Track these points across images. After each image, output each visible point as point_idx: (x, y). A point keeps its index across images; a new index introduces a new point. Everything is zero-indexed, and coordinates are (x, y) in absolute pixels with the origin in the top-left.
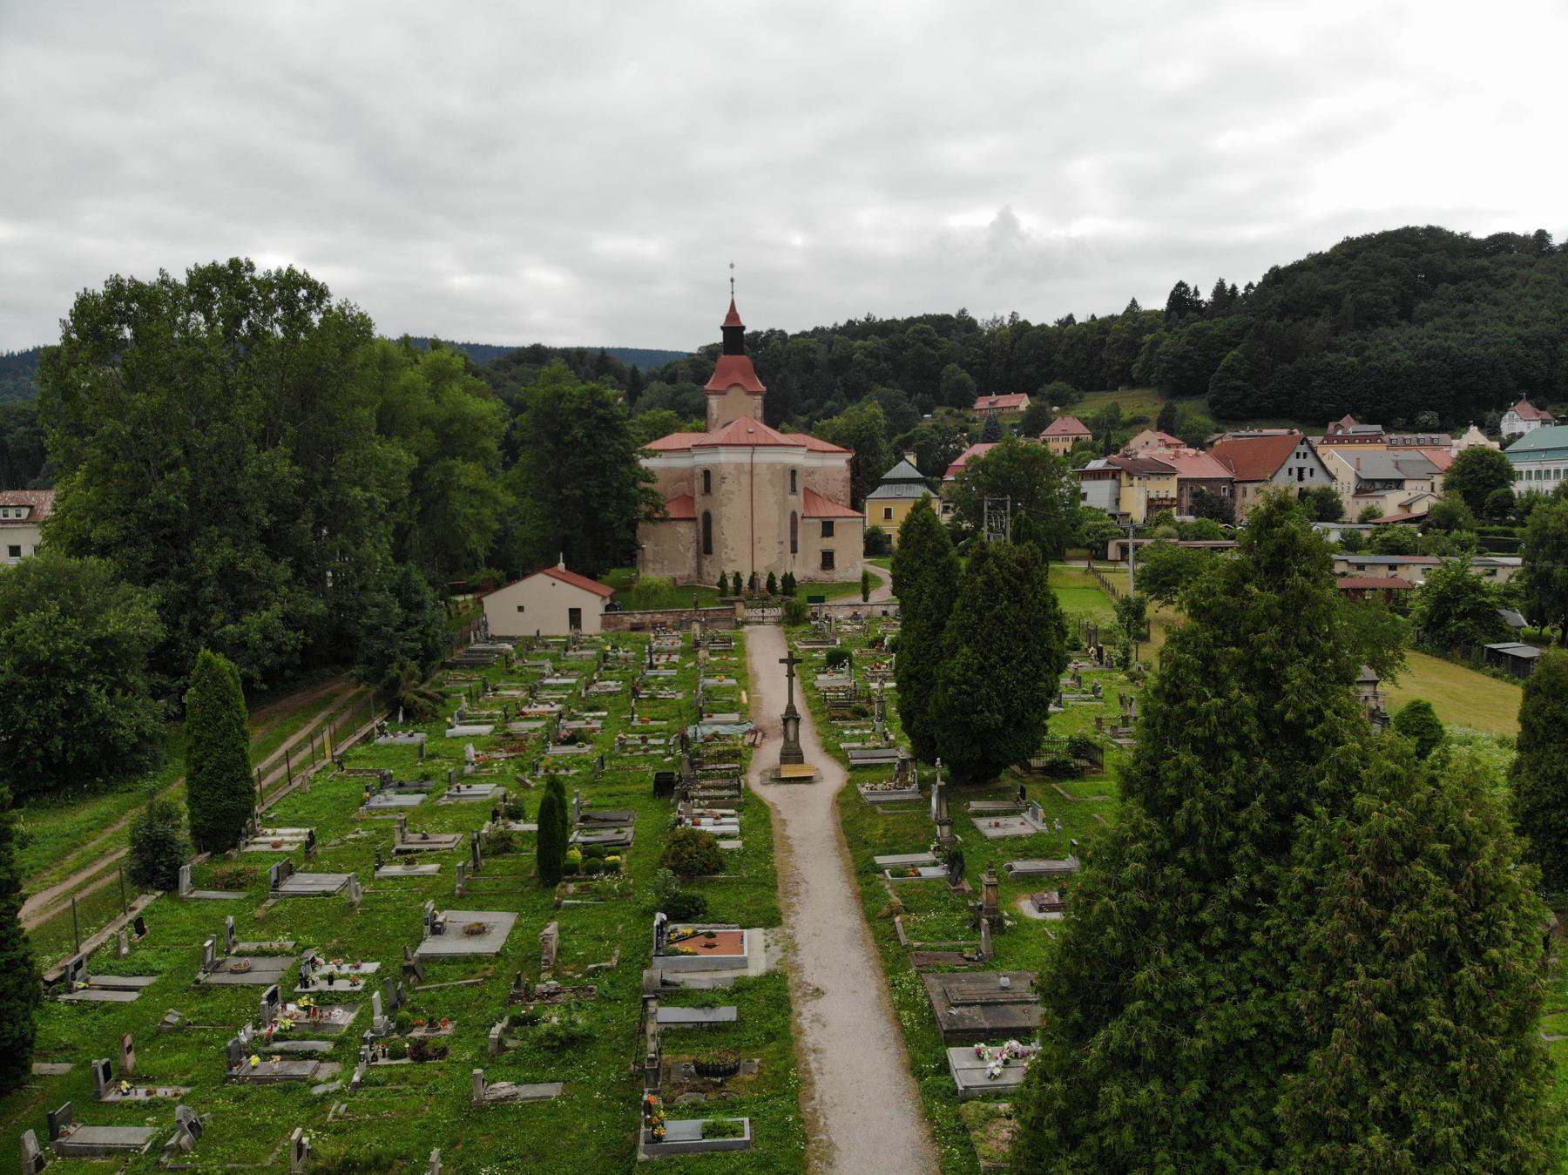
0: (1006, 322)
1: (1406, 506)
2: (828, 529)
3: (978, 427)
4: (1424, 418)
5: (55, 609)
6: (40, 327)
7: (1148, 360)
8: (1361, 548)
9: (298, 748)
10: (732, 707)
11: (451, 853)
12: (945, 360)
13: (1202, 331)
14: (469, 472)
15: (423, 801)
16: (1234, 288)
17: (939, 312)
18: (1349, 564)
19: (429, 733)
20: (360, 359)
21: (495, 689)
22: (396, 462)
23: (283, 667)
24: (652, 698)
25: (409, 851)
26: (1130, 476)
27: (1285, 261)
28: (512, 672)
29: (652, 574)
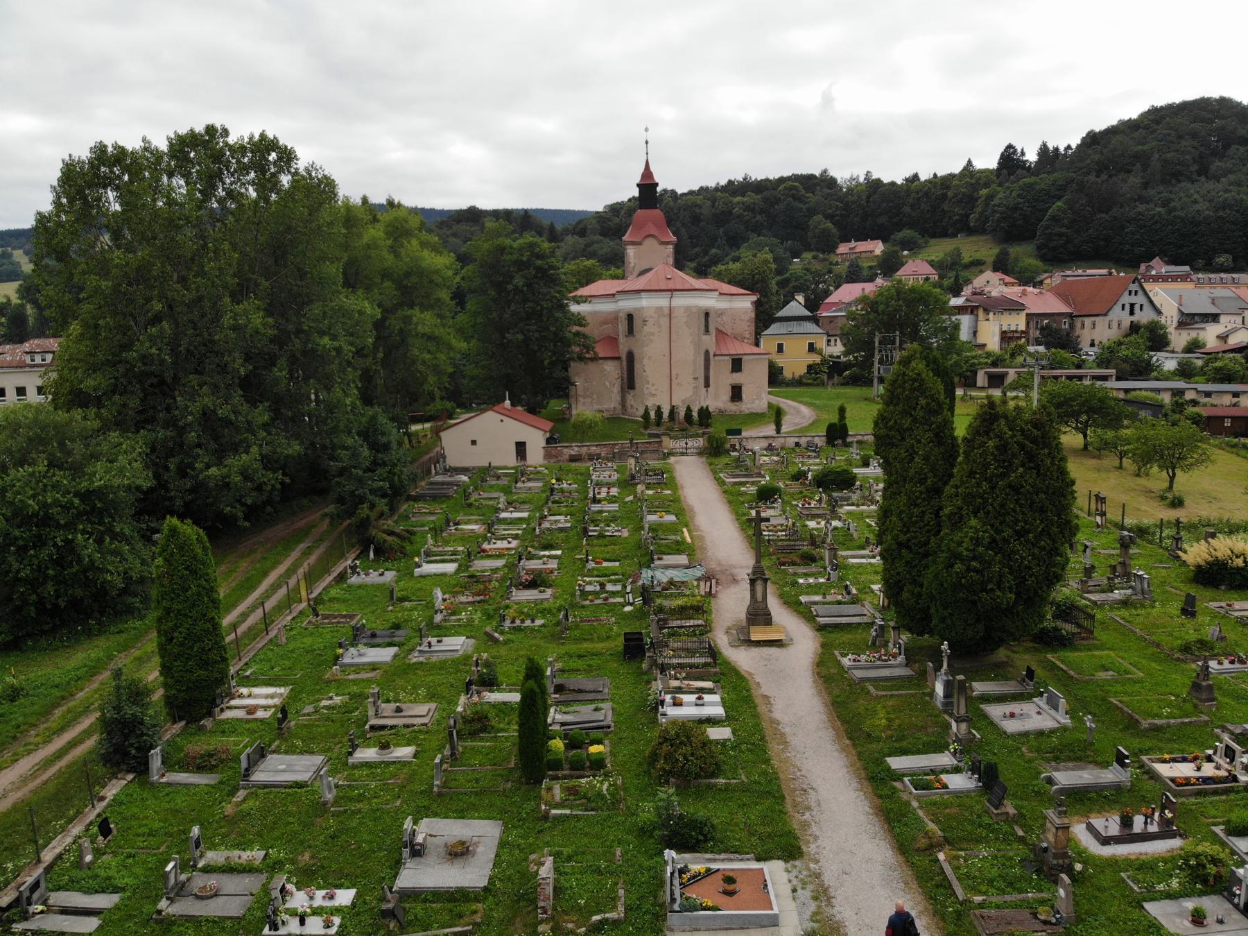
0: (861, 180)
1: (1223, 338)
2: (737, 365)
3: (842, 269)
5: (42, 468)
7: (983, 211)
8: (1195, 375)
9: (274, 588)
10: (679, 547)
11: (426, 729)
12: (812, 212)
13: (1030, 186)
14: (425, 320)
15: (395, 656)
16: (1057, 149)
17: (805, 172)
18: (1198, 392)
19: (398, 571)
21: (457, 524)
22: (360, 313)
23: (265, 504)
24: (601, 536)
25: (383, 727)
26: (986, 311)
27: (1099, 127)
28: (470, 505)
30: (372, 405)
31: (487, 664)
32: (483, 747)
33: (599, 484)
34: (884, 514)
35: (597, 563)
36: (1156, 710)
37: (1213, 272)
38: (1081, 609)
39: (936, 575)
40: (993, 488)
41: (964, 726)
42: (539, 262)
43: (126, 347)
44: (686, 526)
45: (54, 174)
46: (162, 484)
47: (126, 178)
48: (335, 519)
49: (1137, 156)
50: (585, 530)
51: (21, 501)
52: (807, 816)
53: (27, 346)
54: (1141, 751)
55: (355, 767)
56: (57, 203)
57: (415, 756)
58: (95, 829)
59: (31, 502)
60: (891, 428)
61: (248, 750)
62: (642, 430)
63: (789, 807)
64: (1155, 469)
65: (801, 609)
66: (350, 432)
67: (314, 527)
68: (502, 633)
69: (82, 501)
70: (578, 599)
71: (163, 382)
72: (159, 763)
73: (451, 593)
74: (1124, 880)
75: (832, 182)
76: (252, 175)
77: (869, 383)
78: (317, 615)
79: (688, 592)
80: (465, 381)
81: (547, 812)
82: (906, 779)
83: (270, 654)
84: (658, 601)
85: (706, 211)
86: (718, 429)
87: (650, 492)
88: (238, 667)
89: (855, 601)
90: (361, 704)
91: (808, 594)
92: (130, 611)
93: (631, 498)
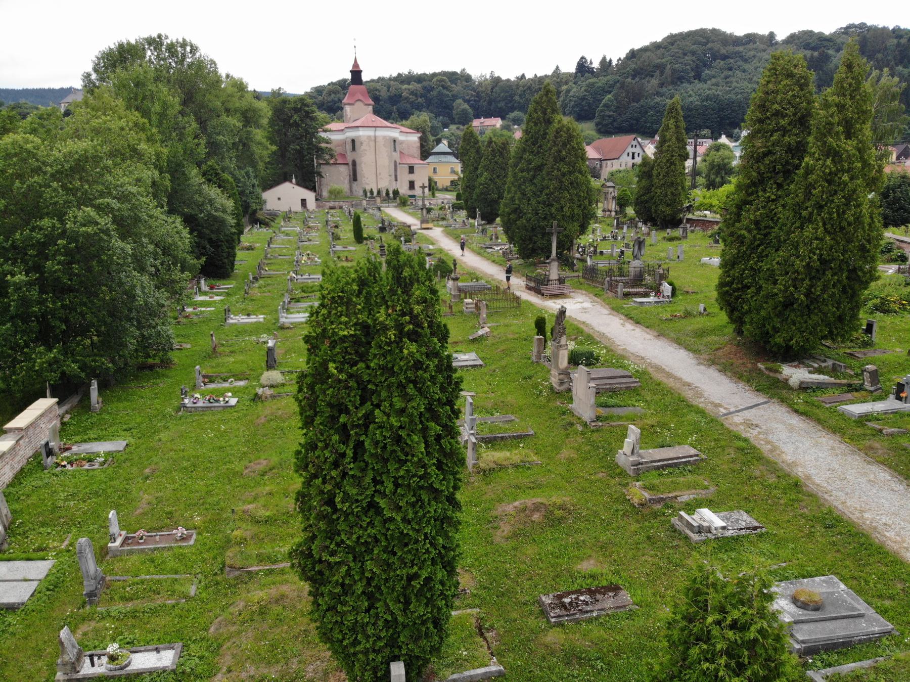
0: (488, 77)
2: (411, 170)
4: (704, 132)
6: (60, 63)
7: (564, 100)
13: (593, 84)
16: (611, 61)
27: (637, 47)
42: (306, 109)
75: (468, 78)
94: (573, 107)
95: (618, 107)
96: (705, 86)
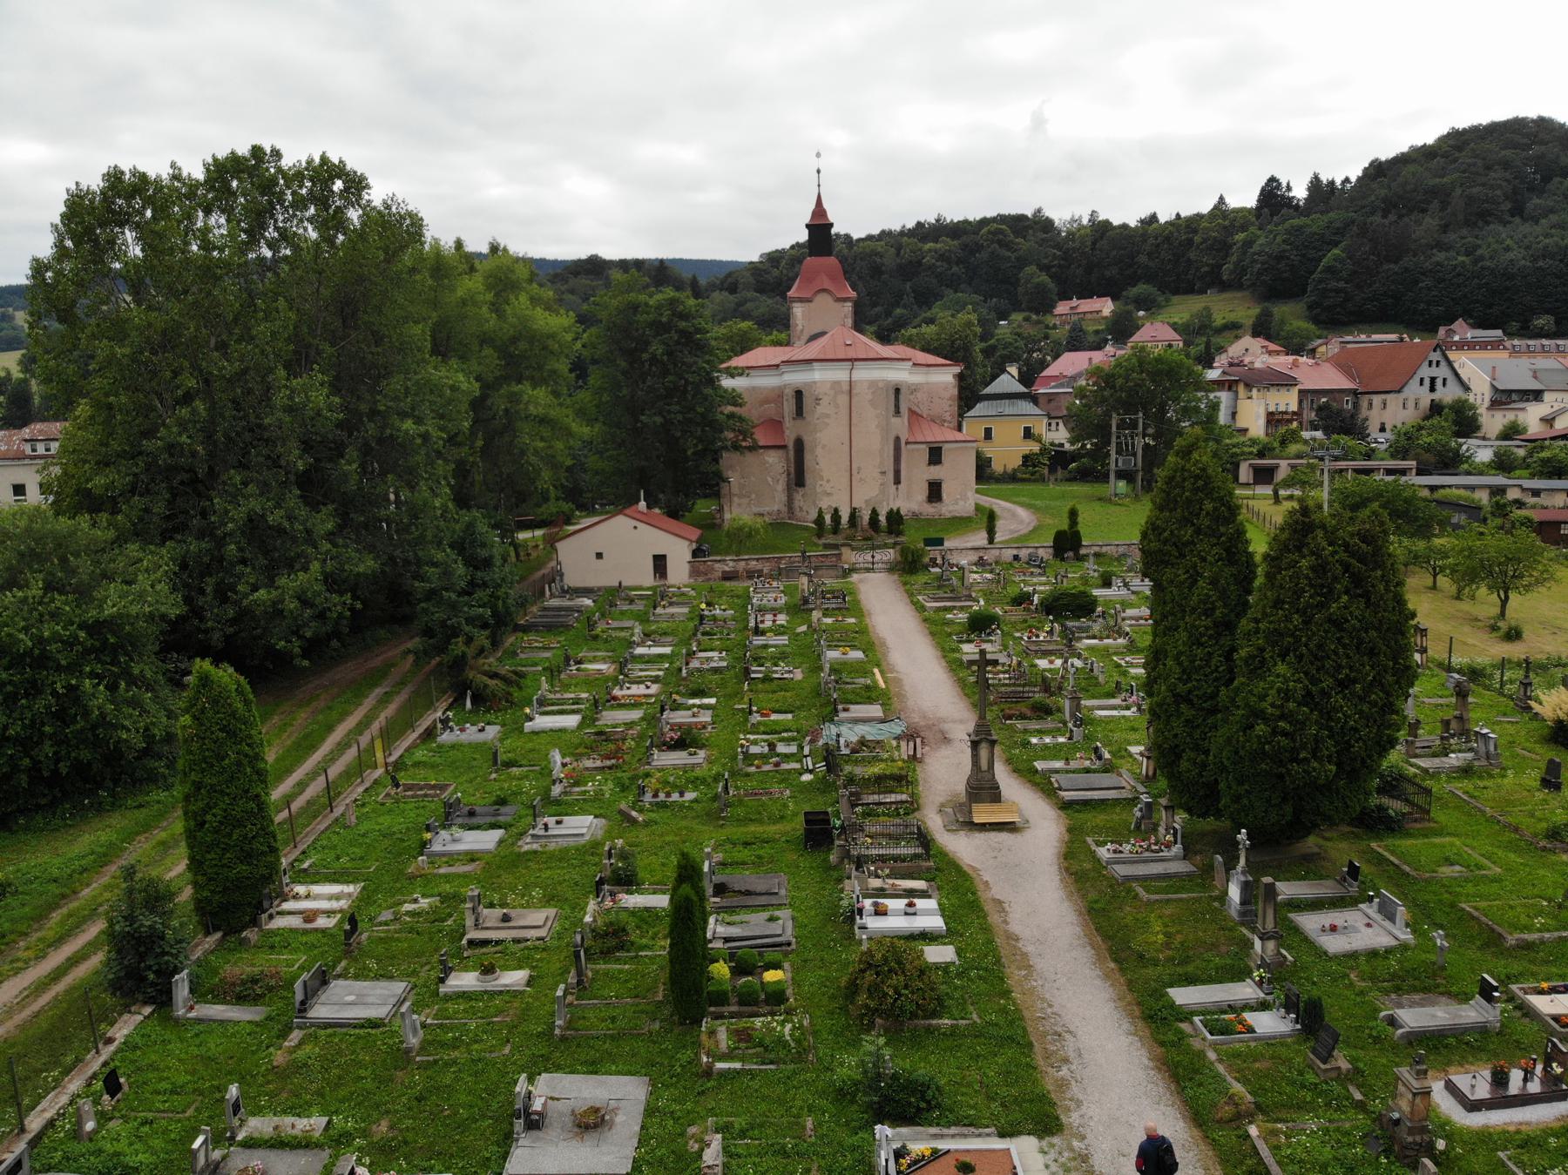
0: (1085, 221)
1: (1548, 421)
2: (935, 456)
3: (1061, 333)
5: (35, 591)
8: (1515, 468)
9: (342, 747)
10: (869, 694)
11: (542, 945)
12: (1022, 262)
13: (1299, 229)
14: (537, 399)
15: (501, 842)
16: (1332, 183)
17: (1013, 212)
18: (1523, 490)
20: (407, 259)
21: (580, 662)
22: (453, 388)
23: (329, 637)
24: (767, 679)
25: (485, 943)
26: (1249, 386)
27: (1386, 153)
28: (595, 638)
29: (739, 512)
30: (469, 508)
31: (623, 856)
32: (620, 971)
33: (761, 610)
34: (1155, 658)
35: (763, 715)
36: (1524, 920)
37: (1530, 338)
38: (1410, 781)
39: (1229, 740)
40: (1305, 623)
41: (1271, 945)
42: (683, 324)
43: (149, 434)
44: (878, 666)
45: (55, 210)
46: (196, 612)
47: (149, 213)
48: (421, 656)
49: (1434, 192)
50: (747, 671)
51: (9, 635)
52: (1064, 1072)
53: (26, 432)
54: (1508, 977)
55: (448, 998)
56: (59, 245)
57: (529, 984)
58: (98, 1085)
59: (22, 636)
60: (1165, 542)
61: (305, 976)
62: (815, 539)
63: (1039, 1060)
64: (1483, 591)
65: (1038, 779)
66: (439, 543)
67: (393, 665)
68: (641, 811)
69: (90, 635)
70: (740, 765)
71: (195, 481)
72: (187, 990)
73: (573, 755)
74: (1504, 1164)
75: (1047, 225)
76: (312, 210)
77: (1103, 478)
78: (397, 785)
79: (886, 756)
80: (587, 477)
81: (710, 1066)
82: (1196, 1019)
83: (335, 839)
84: (848, 768)
85: (890, 260)
86: (913, 538)
87: (829, 621)
88: (292, 857)
89: (1108, 768)
90: (456, 908)
91: (1044, 758)
92: (153, 779)
93: (804, 628)
94: (1259, 273)
95: (1355, 272)
96: (1538, 229)
